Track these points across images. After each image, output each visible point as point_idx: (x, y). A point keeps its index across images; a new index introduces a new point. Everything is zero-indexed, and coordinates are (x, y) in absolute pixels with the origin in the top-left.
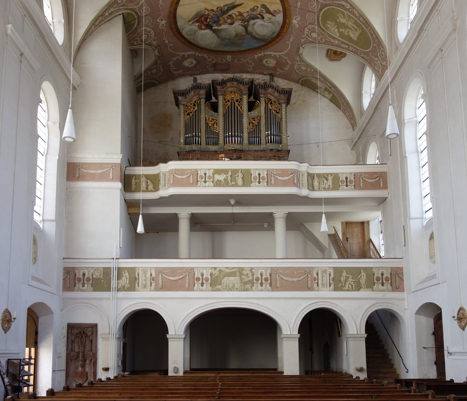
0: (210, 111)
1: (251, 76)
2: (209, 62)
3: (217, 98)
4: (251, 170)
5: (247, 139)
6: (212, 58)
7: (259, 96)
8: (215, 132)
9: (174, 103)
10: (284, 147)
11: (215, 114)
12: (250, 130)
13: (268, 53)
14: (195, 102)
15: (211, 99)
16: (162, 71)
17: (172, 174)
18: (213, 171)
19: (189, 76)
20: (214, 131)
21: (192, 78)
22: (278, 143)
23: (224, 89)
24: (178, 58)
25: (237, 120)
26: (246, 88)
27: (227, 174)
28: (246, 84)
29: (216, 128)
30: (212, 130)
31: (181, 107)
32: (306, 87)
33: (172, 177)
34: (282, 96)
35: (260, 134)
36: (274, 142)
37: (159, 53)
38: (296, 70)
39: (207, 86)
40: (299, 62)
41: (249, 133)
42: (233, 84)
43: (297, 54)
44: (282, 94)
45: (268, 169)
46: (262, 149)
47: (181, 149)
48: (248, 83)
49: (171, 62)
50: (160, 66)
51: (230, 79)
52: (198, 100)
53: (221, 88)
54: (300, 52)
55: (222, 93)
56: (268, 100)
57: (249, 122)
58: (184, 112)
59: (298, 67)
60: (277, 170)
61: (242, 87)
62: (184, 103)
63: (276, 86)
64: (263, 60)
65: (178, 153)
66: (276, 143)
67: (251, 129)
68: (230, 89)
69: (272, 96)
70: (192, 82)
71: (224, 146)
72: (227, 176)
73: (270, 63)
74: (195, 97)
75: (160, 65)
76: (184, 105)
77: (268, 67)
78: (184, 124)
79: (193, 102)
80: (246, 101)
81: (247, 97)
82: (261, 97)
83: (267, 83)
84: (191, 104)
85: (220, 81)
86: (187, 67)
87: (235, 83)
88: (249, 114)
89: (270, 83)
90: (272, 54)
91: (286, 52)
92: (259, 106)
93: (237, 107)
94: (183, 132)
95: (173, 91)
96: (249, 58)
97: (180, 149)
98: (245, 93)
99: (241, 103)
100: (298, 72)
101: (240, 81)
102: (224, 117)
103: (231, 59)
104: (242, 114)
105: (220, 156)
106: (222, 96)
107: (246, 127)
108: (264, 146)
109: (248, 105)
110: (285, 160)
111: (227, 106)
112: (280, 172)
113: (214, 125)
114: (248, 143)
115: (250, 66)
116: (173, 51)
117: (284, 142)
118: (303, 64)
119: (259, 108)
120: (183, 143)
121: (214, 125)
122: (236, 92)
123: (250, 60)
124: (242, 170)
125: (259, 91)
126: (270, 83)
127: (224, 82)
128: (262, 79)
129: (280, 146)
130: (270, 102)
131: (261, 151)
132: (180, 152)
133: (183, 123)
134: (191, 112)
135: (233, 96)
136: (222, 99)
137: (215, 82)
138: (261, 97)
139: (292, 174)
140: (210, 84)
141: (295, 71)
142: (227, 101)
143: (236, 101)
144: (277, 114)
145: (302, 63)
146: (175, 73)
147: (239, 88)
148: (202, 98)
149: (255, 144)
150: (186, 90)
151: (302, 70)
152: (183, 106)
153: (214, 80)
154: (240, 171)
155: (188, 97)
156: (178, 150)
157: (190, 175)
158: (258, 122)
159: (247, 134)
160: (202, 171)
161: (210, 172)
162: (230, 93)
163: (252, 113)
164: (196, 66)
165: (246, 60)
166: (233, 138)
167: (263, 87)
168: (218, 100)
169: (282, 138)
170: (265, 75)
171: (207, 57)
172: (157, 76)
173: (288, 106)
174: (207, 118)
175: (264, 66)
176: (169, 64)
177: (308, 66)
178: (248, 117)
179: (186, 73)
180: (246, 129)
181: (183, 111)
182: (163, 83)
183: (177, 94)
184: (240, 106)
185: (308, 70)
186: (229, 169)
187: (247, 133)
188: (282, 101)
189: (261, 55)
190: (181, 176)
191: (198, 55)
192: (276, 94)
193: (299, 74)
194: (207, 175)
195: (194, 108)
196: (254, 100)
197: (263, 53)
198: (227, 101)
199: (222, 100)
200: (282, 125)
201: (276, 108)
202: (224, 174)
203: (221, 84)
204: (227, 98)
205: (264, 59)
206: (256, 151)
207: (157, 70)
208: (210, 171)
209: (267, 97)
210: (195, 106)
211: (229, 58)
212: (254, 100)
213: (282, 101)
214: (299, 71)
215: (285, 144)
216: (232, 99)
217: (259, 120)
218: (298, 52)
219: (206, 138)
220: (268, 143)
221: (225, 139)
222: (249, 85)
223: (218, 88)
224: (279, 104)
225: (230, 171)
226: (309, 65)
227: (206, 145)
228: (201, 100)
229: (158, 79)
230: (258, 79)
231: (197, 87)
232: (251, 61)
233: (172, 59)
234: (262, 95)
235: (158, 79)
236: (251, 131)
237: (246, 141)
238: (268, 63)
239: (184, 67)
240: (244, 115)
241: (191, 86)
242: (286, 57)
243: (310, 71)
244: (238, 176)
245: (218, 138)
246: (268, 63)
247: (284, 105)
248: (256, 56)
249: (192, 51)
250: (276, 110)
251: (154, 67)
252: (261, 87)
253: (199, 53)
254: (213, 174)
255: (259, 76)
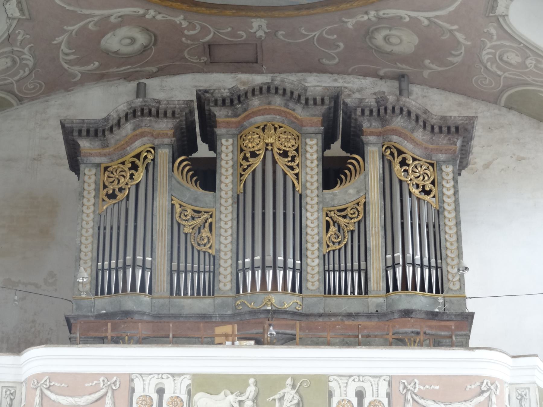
0: (189, 186)
1: (336, 80)
2: (188, 37)
3: (213, 147)
4: (331, 378)
5: (317, 277)
6: (203, 28)
7: (362, 141)
8: (205, 252)
9: (66, 162)
10: (451, 302)
11: (208, 196)
12: (328, 246)
13: (392, 12)
14: (138, 156)
15: (195, 150)
16: (31, 63)
17: (38, 392)
18: (189, 382)
19: (121, 81)
20: (199, 251)
21: (133, 85)
22: (430, 291)
23: (239, 118)
24: (85, 27)
25: (264, 214)
26: (315, 115)
27: (242, 393)
28: (315, 103)
29: (209, 240)
30: (193, 247)
31: (87, 171)
32: (526, 119)
33: (37, 400)
34: (443, 140)
35: (366, 261)
36: (414, 288)
37: (21, 10)
38: (489, 64)
39: (182, 110)
40: (499, 39)
41: (325, 258)
42: (269, 103)
43: (488, 17)
44: (443, 136)
45: (391, 377)
46: (372, 310)
47: (79, 307)
48: (323, 100)
49: (62, 39)
50: (24, 49)
51: (261, 89)
52: (148, 151)
53: (227, 116)
54: (500, 10)
55: (233, 131)
56: (392, 154)
57: (327, 222)
58: (97, 190)
59: (494, 55)
60: (425, 379)
61: (299, 112)
62: (97, 160)
63: (419, 109)
64: (372, 32)
65: (68, 320)
66: (423, 289)
67: (334, 243)
68: (259, 120)
69: (404, 139)
70: (132, 97)
71: (236, 299)
72: (239, 398)
73: (399, 41)
74: (138, 143)
75: (22, 45)
76: (98, 165)
77: (390, 53)
78: (93, 228)
79: (129, 158)
80: (315, 156)
81: (320, 144)
82: (368, 143)
83: (387, 99)
84: (123, 163)
85: (225, 95)
86: (116, 53)
87: (278, 101)
88: (327, 196)
89: (398, 100)
90: (403, 15)
91: (451, 8)
92: (360, 169)
93: (285, 175)
94: (92, 251)
95: (63, 126)
96: (328, 27)
97: (75, 307)
98: (311, 129)
99: (297, 160)
100: (494, 69)
101: (295, 95)
102: (236, 206)
103: (267, 31)
104: (301, 195)
105: (219, 330)
106: (231, 141)
107: (316, 238)
108: (381, 300)
109: (321, 167)
110: (452, 345)
111: (250, 171)
112: (437, 388)
113: (199, 228)
114: (322, 289)
115: (332, 52)
116: (69, 4)
117: (451, 286)
118: (511, 47)
119: (362, 177)
120: (88, 287)
121: (199, 228)
122: (280, 127)
123: (330, 32)
124: (295, 378)
125: (361, 126)
126: (398, 100)
127: (239, 97)
128: (372, 91)
129: (436, 300)
130: (398, 160)
131: (369, 316)
132: (76, 318)
133: (91, 224)
134: (121, 190)
135: (270, 140)
136: (231, 148)
137: (208, 95)
138: (368, 143)
139: (483, 392)
140: (189, 103)
141: (486, 67)
142: (248, 155)
143: (280, 154)
144: (427, 198)
145: (507, 43)
146: (76, 70)
147: (292, 115)
148: (163, 145)
149: (346, 293)
150: (106, 119)
151: (507, 63)
152: (94, 171)
153: (206, 91)
154: (289, 381)
155: (112, 141)
156: (69, 310)
157: (106, 394)
158: (359, 222)
159: (317, 261)
160: (147, 382)
161: (178, 385)
162: (260, 131)
163: (335, 195)
164: (145, 49)
165: (317, 33)
166: (270, 274)
167: (375, 113)
168: (218, 151)
169: (445, 273)
170: (381, 78)
171: (185, 24)
172: (10, 80)
173: (463, 172)
174: (178, 209)
175: (379, 50)
176: (55, 42)
177: (529, 53)
178: (321, 206)
179: (111, 70)
180: (316, 246)
181: (93, 186)
182: (32, 99)
183: (76, 134)
184: (296, 172)
185: (530, 62)
186: (249, 376)
187: (318, 257)
188: (442, 157)
189: (369, 19)
190: (71, 396)
191: (154, 17)
192: (420, 135)
193: (500, 76)
194: (166, 396)
195: (132, 176)
196: (343, 154)
197: (372, 13)
198: (248, 155)
199: (233, 151)
200: (442, 234)
201: (421, 178)
202: (228, 392)
203: (228, 102)
204: (250, 145)
205: (377, 30)
206: (350, 315)
207: (14, 61)
208: (178, 380)
209: (389, 144)
210: (137, 171)
211: (260, 27)
212: (343, 154)
213: (442, 157)
214: (499, 68)
215: (455, 294)
216: (267, 150)
217: (361, 216)
218: (493, 8)
219: (171, 271)
220: (395, 288)
221: (241, 275)
222: (326, 107)
223: (217, 114)
224: (432, 165)
225: (251, 381)
226: (530, 49)
227: (172, 293)
228: (160, 151)
229: (15, 87)
230: (360, 90)
231: (146, 111)
232: (335, 36)
233: (65, 27)
234: (372, 139)
235: (15, 87)
236: (334, 251)
237: (317, 284)
238: (391, 44)
239: (107, 52)
240: (308, 199)
241: (123, 108)
242: (452, 25)
243: (536, 67)
244: (281, 399)
245: (214, 273)
246: (391, 44)
247: (448, 170)
248: (350, 23)
249: (133, 6)
250: (421, 183)
251: (5, 53)
252: (367, 113)
253: (156, 11)
254: (189, 393)
255: (363, 81)
